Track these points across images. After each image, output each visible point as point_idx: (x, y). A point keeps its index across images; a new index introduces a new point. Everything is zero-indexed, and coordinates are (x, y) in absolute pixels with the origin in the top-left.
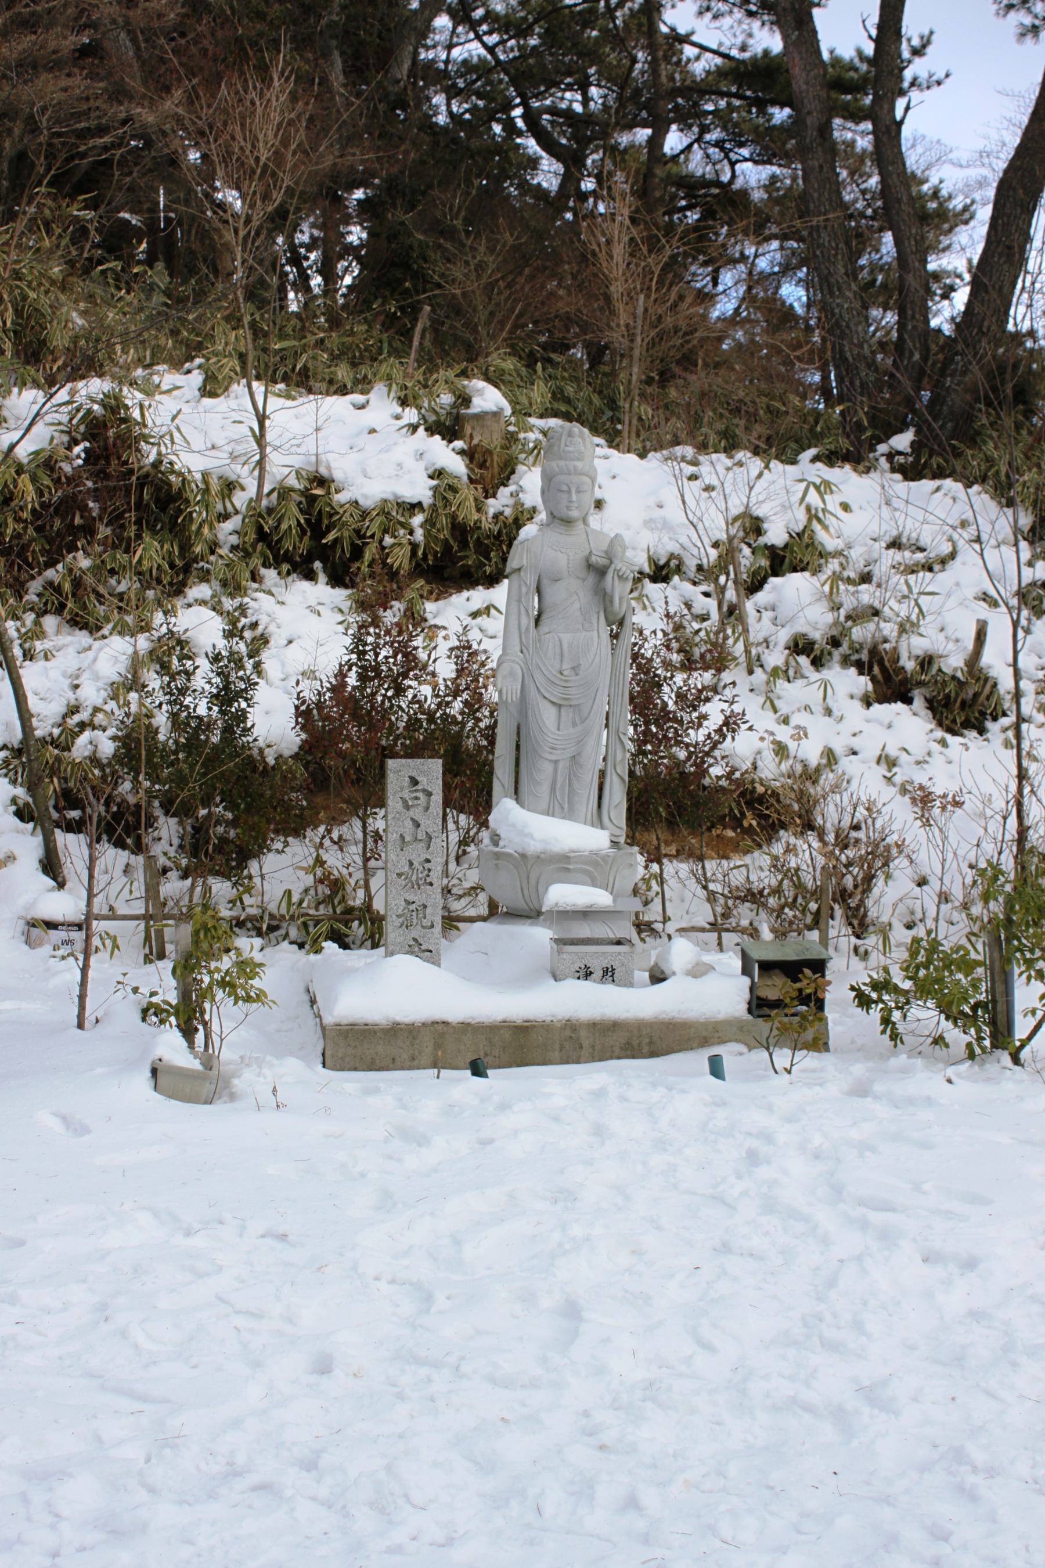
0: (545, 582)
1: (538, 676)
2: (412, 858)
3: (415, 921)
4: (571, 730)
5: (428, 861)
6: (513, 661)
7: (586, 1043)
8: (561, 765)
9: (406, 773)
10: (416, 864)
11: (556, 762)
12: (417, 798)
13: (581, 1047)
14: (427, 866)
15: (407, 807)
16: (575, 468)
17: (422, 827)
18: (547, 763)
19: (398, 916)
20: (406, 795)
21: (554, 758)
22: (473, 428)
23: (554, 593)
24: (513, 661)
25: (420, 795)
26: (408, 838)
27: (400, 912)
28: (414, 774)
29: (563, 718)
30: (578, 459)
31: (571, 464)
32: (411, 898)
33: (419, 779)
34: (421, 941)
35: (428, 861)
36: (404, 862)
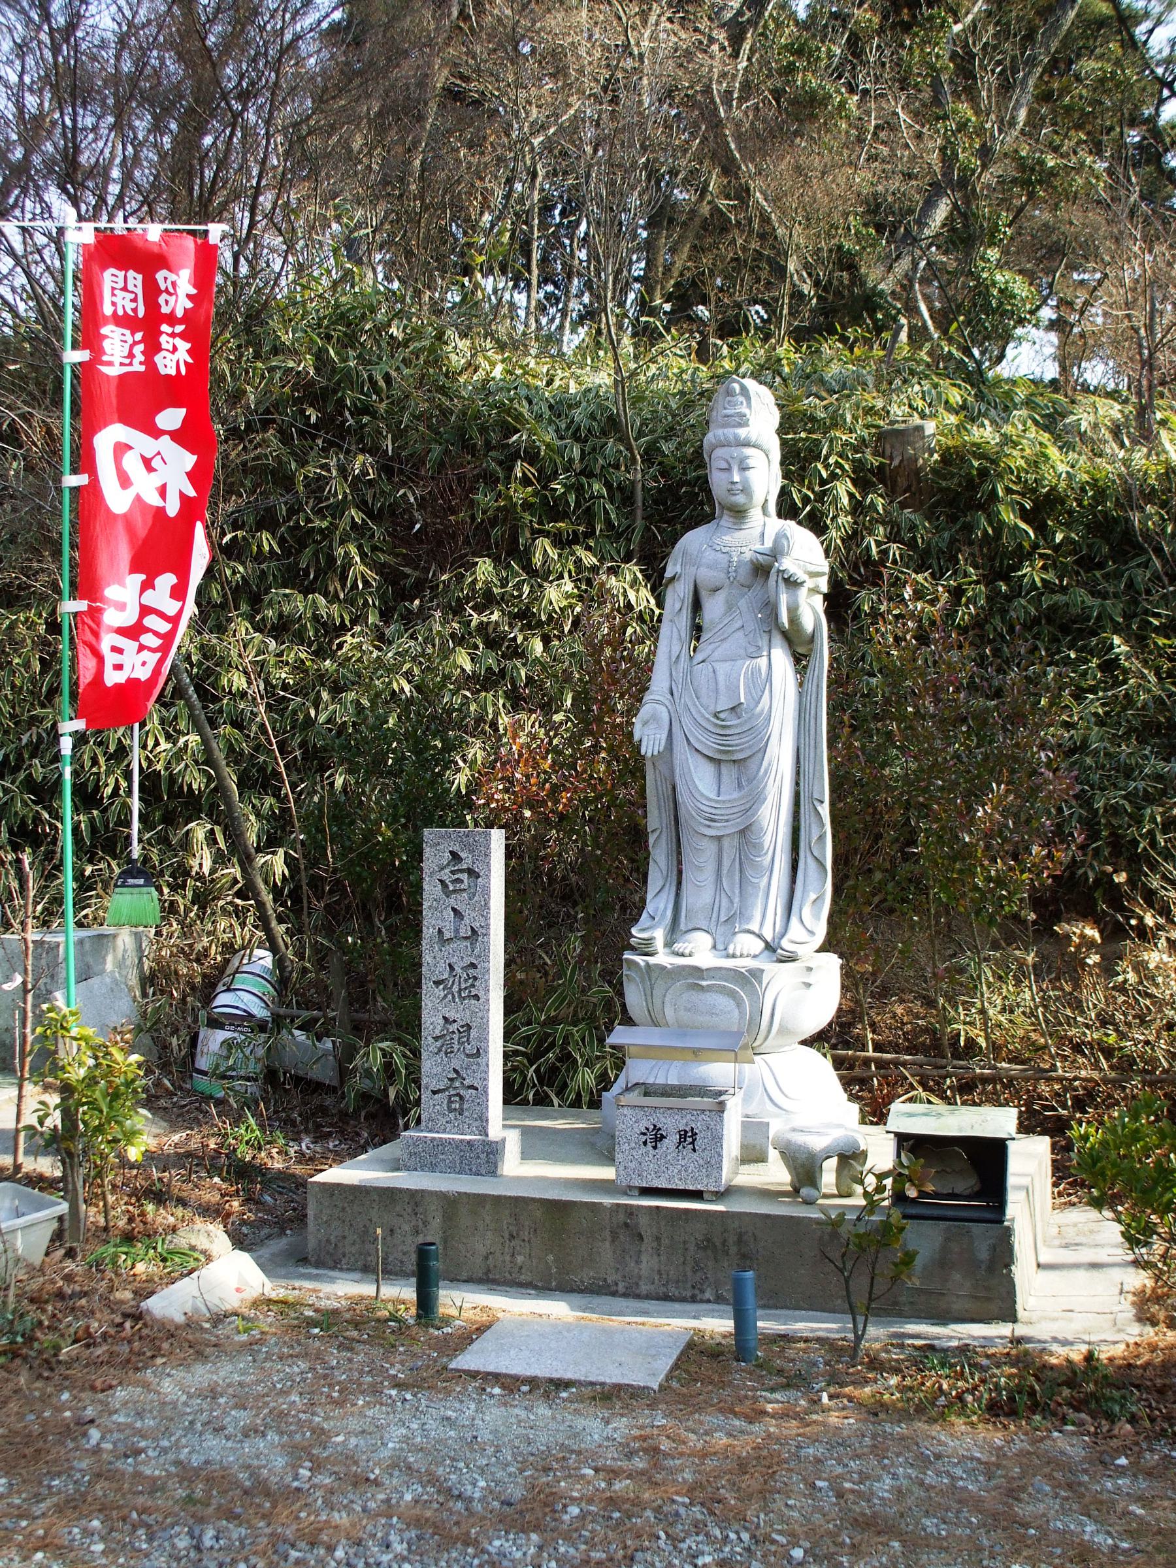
0: (703, 594)
1: (687, 721)
2: (453, 961)
3: (456, 1047)
4: (735, 795)
5: (473, 966)
6: (657, 702)
7: (647, 1234)
8: (726, 843)
9: (446, 847)
10: (458, 969)
11: (719, 838)
12: (460, 881)
13: (641, 1237)
14: (471, 972)
15: (448, 894)
16: (736, 437)
17: (467, 920)
18: (705, 843)
19: (436, 1039)
20: (446, 875)
21: (713, 833)
22: (892, 447)
23: (713, 608)
24: (657, 702)
25: (464, 876)
26: (447, 935)
27: (437, 1033)
28: (456, 848)
29: (725, 778)
30: (740, 425)
31: (742, 432)
32: (451, 1015)
33: (462, 855)
34: (463, 1073)
35: (473, 966)
36: (442, 966)
